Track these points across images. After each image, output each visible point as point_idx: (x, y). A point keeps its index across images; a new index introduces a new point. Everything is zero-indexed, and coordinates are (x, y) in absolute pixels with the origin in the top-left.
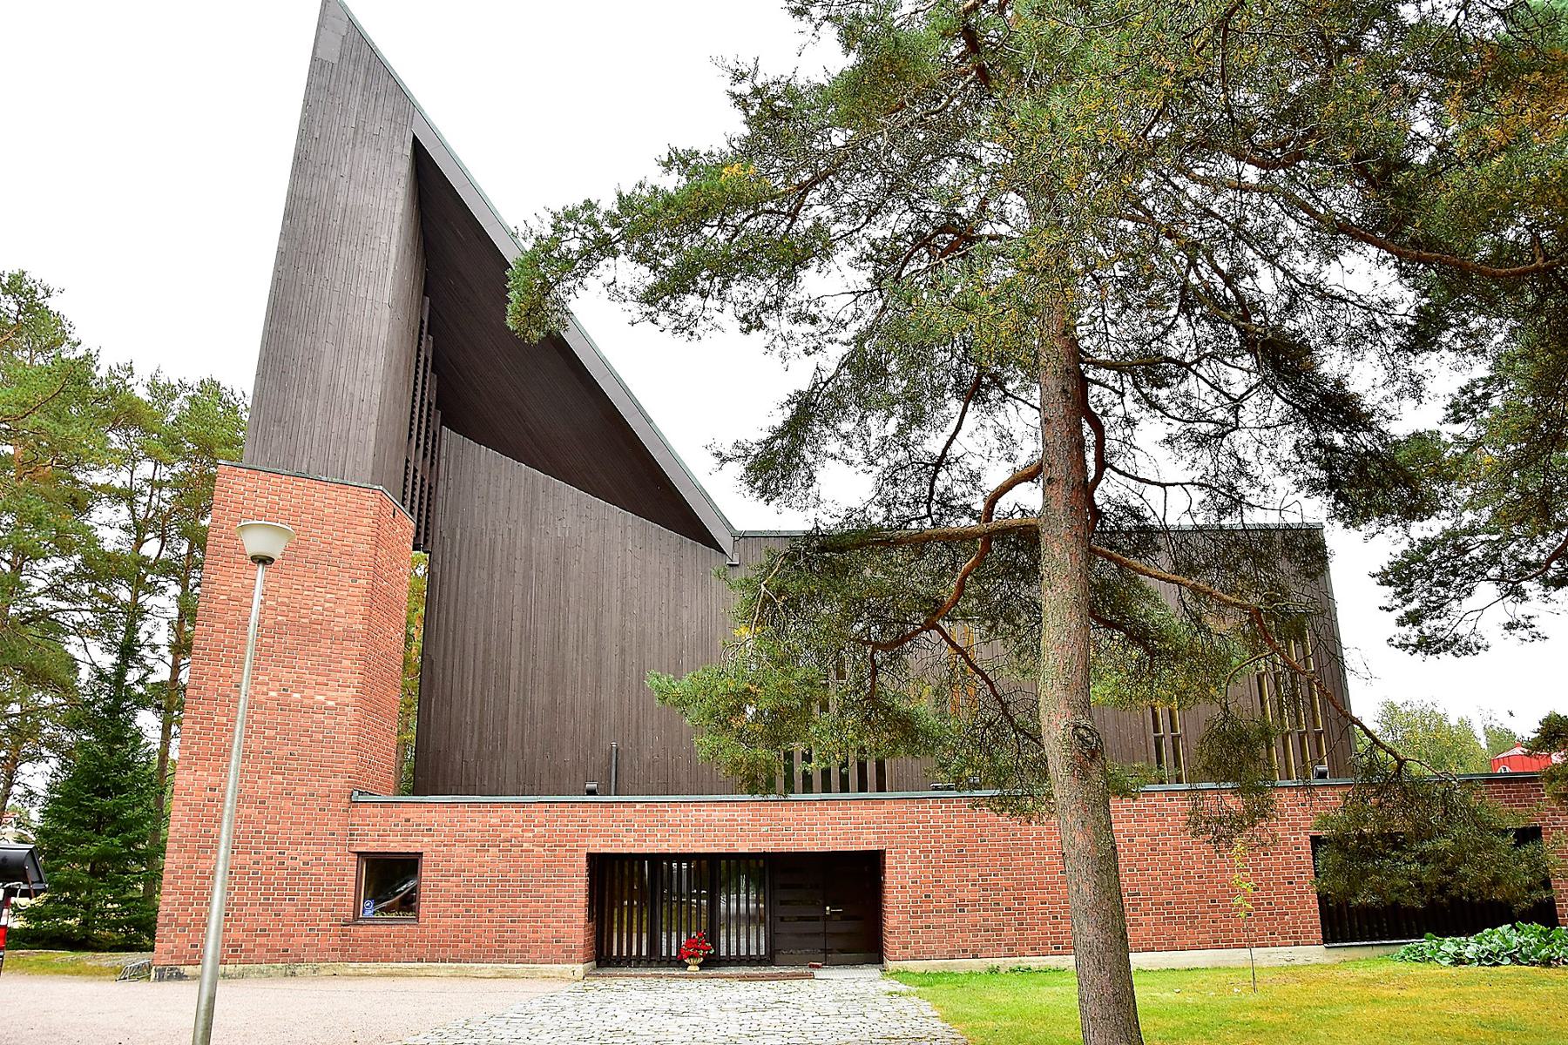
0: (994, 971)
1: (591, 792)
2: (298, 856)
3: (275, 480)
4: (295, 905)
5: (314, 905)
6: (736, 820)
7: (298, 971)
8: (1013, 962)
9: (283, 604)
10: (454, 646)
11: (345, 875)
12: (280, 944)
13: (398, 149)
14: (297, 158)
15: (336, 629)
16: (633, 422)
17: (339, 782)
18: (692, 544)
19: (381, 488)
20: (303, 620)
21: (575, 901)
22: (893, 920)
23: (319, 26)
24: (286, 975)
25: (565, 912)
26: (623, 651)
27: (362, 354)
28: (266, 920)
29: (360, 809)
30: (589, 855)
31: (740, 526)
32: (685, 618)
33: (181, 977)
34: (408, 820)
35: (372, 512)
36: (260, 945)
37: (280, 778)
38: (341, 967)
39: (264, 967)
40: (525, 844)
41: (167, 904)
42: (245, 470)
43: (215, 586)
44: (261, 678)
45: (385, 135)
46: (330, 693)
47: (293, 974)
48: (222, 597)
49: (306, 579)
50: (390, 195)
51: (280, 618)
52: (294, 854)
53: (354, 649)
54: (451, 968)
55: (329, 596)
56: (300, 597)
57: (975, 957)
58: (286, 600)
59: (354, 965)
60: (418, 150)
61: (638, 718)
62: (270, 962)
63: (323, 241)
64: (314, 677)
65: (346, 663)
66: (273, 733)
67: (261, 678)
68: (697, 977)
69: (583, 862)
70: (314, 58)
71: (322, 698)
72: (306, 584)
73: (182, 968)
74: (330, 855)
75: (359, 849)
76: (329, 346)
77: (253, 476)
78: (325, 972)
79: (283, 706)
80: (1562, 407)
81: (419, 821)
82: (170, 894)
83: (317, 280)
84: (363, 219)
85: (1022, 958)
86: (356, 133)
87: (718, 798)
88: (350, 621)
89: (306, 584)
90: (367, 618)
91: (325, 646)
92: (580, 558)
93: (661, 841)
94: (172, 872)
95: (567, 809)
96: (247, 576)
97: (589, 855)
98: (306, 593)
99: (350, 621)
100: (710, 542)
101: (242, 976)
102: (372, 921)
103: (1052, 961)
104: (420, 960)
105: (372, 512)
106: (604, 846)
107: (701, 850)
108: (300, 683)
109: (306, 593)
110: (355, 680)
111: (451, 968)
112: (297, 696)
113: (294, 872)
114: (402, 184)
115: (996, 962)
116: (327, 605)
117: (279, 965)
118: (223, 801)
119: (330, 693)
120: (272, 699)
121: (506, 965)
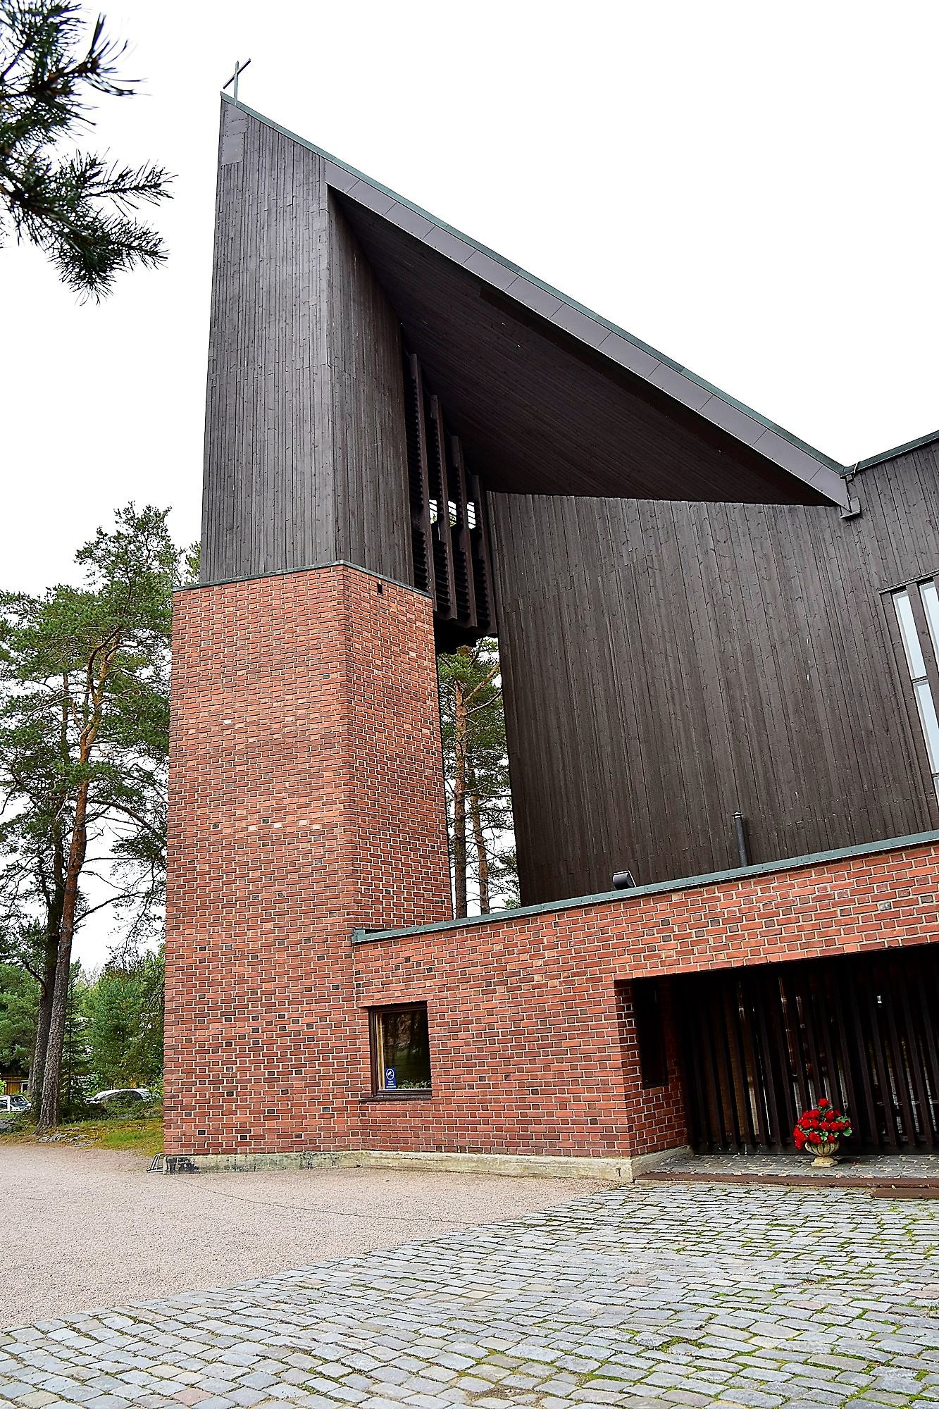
1: (622, 885)
2: (302, 1017)
3: (229, 590)
5: (325, 1078)
7: (315, 1161)
10: (537, 736)
12: (292, 1126)
13: (314, 208)
14: (216, 266)
15: (313, 738)
16: (656, 380)
17: (338, 919)
19: (342, 562)
20: (275, 736)
23: (221, 137)
24: (301, 1167)
25: (598, 1075)
26: (728, 685)
27: (307, 427)
28: (273, 1099)
29: (362, 951)
30: (618, 984)
31: (848, 459)
33: (192, 1169)
34: (407, 960)
35: (335, 593)
37: (270, 925)
39: (276, 1157)
40: (537, 978)
41: (170, 1084)
42: (199, 590)
43: (185, 722)
44: (238, 812)
45: (300, 201)
46: (313, 816)
47: (310, 1166)
48: (191, 732)
49: (273, 689)
50: (312, 256)
51: (250, 740)
52: (295, 1015)
53: (336, 755)
54: (471, 1160)
55: (300, 701)
59: (376, 1154)
60: (339, 202)
61: (765, 774)
62: (283, 1150)
63: (252, 330)
64: (295, 800)
67: (238, 812)
68: (831, 1183)
69: (612, 991)
70: (220, 167)
72: (274, 694)
73: (192, 1159)
75: (369, 1004)
76: (271, 432)
77: (207, 594)
78: (346, 1163)
79: (265, 839)
81: (419, 958)
83: (251, 372)
84: (289, 292)
86: (269, 214)
89: (274, 694)
90: (348, 717)
91: (303, 761)
92: (655, 582)
93: (715, 949)
95: (581, 917)
96: (213, 702)
97: (618, 984)
98: (275, 704)
99: (326, 725)
100: (812, 497)
101: (254, 1168)
102: (390, 1097)
104: (439, 1149)
105: (335, 593)
106: (637, 968)
107: (780, 958)
108: (280, 809)
109: (275, 704)
111: (471, 1160)
112: (277, 825)
113: (297, 1037)
114: (324, 238)
117: (293, 1155)
119: (313, 816)
120: (251, 835)
121: (532, 1158)
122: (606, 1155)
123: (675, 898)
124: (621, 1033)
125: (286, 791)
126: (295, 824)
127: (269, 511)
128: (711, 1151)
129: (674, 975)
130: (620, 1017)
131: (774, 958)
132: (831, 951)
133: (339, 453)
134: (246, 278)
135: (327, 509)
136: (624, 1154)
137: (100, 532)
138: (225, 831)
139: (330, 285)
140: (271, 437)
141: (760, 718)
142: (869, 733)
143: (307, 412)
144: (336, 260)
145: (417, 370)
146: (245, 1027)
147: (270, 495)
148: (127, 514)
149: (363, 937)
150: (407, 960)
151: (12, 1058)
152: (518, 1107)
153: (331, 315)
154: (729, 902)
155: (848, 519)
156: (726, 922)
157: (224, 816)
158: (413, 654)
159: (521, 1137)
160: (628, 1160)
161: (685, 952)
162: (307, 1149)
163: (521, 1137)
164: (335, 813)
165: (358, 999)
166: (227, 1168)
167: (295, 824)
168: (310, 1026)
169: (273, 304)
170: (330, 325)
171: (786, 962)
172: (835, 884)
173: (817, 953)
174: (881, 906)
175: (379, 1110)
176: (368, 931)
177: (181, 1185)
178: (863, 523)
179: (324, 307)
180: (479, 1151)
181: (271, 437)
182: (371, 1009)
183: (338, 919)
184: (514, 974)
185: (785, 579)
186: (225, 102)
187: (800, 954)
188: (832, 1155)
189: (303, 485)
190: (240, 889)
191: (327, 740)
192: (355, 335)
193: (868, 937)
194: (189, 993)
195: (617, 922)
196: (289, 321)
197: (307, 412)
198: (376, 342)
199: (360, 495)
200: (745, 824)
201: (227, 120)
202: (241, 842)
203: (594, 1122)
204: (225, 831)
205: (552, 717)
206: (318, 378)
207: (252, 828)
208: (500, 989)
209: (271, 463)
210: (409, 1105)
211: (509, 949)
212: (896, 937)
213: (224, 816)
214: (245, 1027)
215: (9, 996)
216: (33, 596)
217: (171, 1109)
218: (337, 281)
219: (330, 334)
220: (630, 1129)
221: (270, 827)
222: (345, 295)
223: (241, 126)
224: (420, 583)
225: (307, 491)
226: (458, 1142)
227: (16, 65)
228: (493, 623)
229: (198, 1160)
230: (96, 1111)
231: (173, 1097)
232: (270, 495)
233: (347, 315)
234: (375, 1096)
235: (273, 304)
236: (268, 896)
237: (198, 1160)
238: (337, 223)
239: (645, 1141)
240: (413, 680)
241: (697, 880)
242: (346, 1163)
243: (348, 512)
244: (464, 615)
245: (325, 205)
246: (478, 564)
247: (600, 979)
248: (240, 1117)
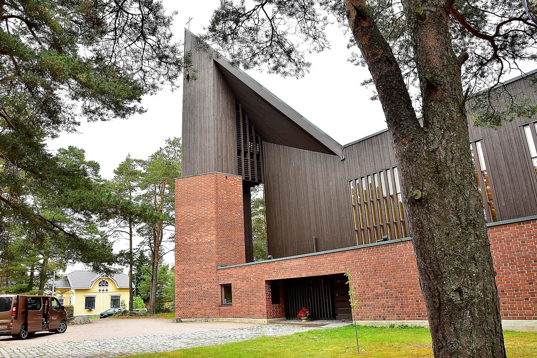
0: (392, 326)
1: (270, 259)
2: (206, 287)
4: (206, 301)
6: (301, 265)
8: (400, 322)
9: (194, 214)
11: (218, 291)
15: (208, 218)
17: (213, 264)
18: (330, 156)
21: (264, 297)
22: (354, 303)
28: (199, 305)
30: (266, 281)
31: (343, 144)
32: (331, 184)
33: (181, 322)
36: (199, 313)
37: (199, 265)
38: (221, 319)
40: (252, 279)
41: (176, 302)
43: (178, 213)
44: (191, 237)
47: (207, 321)
53: (214, 223)
54: (239, 320)
56: (198, 211)
57: (384, 319)
58: (195, 213)
59: (221, 318)
65: (212, 228)
66: (196, 252)
67: (191, 237)
71: (207, 240)
74: (213, 286)
75: (220, 284)
76: (199, 134)
78: (215, 321)
80: (276, 0)
82: (177, 299)
83: (193, 117)
85: (404, 321)
87: (337, 250)
88: (212, 215)
94: (176, 293)
97: (266, 281)
99: (212, 215)
101: (195, 321)
103: (417, 323)
108: (201, 236)
110: (215, 232)
111: (239, 320)
112: (200, 240)
115: (393, 322)
116: (205, 212)
118: (8, 298)
120: (194, 242)
121: (250, 319)
123: (276, 262)
124: (266, 292)
126: (204, 240)
127: (198, 157)
128: (290, 319)
129: (291, 278)
130: (266, 288)
131: (292, 277)
133: (216, 140)
134: (192, 89)
135: (213, 157)
137: (161, 148)
138: (188, 241)
139: (214, 91)
140: (199, 136)
141: (321, 211)
142: (343, 218)
143: (207, 129)
144: (215, 82)
145: (240, 109)
146: (192, 289)
147: (198, 153)
148: (169, 141)
149: (220, 267)
150: (228, 274)
151: (147, 297)
152: (248, 308)
153: (214, 99)
154: (285, 265)
155: (342, 160)
158: (236, 194)
159: (248, 314)
160: (266, 319)
162: (207, 317)
163: (248, 314)
164: (213, 237)
166: (189, 321)
167: (204, 240)
168: (208, 289)
169: (199, 96)
170: (213, 103)
171: (286, 279)
172: (302, 262)
173: (298, 277)
175: (222, 308)
176: (221, 266)
177: (180, 324)
179: (212, 97)
180: (241, 318)
181: (199, 136)
185: (328, 175)
186: (186, 32)
187: (296, 277)
188: (306, 320)
189: (207, 150)
190: (192, 256)
191: (252, 191)
192: (221, 103)
193: (307, 274)
195: (266, 268)
196: (203, 102)
197: (207, 129)
198: (228, 104)
199: (222, 151)
200: (316, 240)
201: (187, 37)
202: (192, 244)
203: (261, 311)
204: (188, 241)
205: (276, 207)
206: (210, 119)
207: (194, 241)
208: (245, 281)
209: (199, 143)
210: (228, 307)
212: (311, 274)
214: (192, 289)
215: (146, 276)
216: (145, 160)
217: (177, 308)
218: (216, 88)
219: (213, 106)
220: (267, 313)
222: (218, 92)
223: (190, 39)
224: (240, 173)
225: (208, 151)
226: (237, 316)
227: (129, 239)
228: (263, 180)
229: (183, 320)
230: (168, 311)
232: (198, 153)
233: (218, 98)
234: (222, 305)
235: (199, 96)
237: (183, 320)
238: (216, 70)
239: (272, 316)
240: (236, 201)
241: (310, 254)
242: (215, 321)
243: (218, 157)
244: (254, 179)
245: (212, 65)
246: (259, 163)
247: (263, 280)
248: (192, 310)
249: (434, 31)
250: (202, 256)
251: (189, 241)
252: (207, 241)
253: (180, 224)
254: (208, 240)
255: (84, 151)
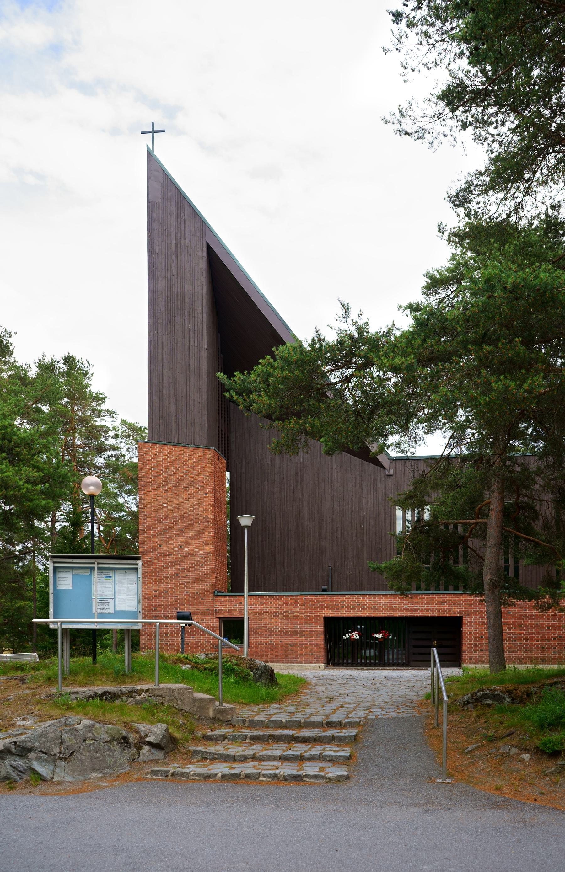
1: (324, 590)
5: (203, 640)
9: (175, 507)
17: (209, 586)
30: (325, 618)
37: (183, 586)
46: (200, 548)
58: (177, 506)
65: (206, 533)
82: (143, 635)
97: (325, 618)
107: (376, 616)
108: (187, 544)
112: (186, 549)
116: (195, 507)
120: (176, 551)
121: (289, 664)
122: (315, 663)
125: (190, 537)
126: (193, 550)
132: (390, 615)
136: (322, 663)
154: (364, 600)
156: (362, 605)
157: (164, 542)
161: (348, 611)
165: (216, 614)
173: (387, 615)
174: (405, 606)
178: (392, 478)
182: (220, 618)
183: (209, 586)
184: (286, 611)
191: (206, 520)
194: (150, 607)
202: (171, 554)
207: (176, 549)
211: (286, 603)
212: (408, 614)
213: (164, 542)
221: (183, 549)
231: (144, 644)
236: (182, 575)
249: (308, 429)
250: (189, 573)
251: (167, 548)
252: (198, 552)
253: (149, 519)
254: (200, 550)
255: (424, 275)
